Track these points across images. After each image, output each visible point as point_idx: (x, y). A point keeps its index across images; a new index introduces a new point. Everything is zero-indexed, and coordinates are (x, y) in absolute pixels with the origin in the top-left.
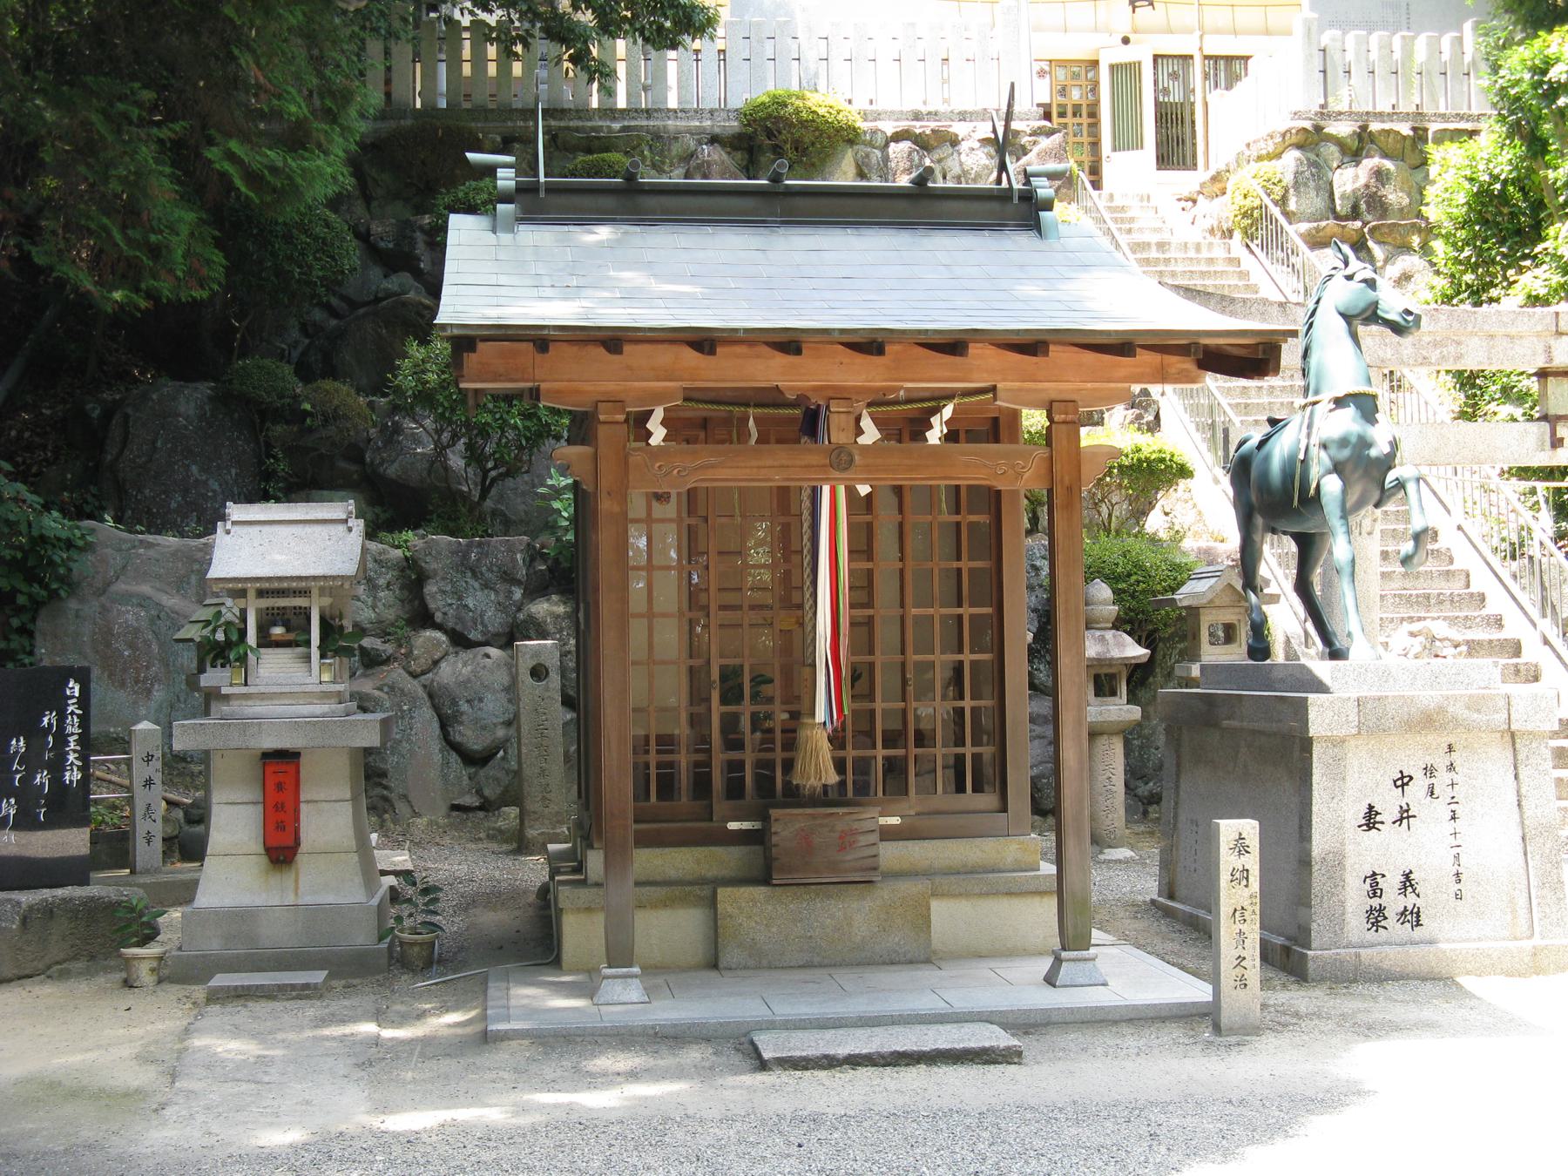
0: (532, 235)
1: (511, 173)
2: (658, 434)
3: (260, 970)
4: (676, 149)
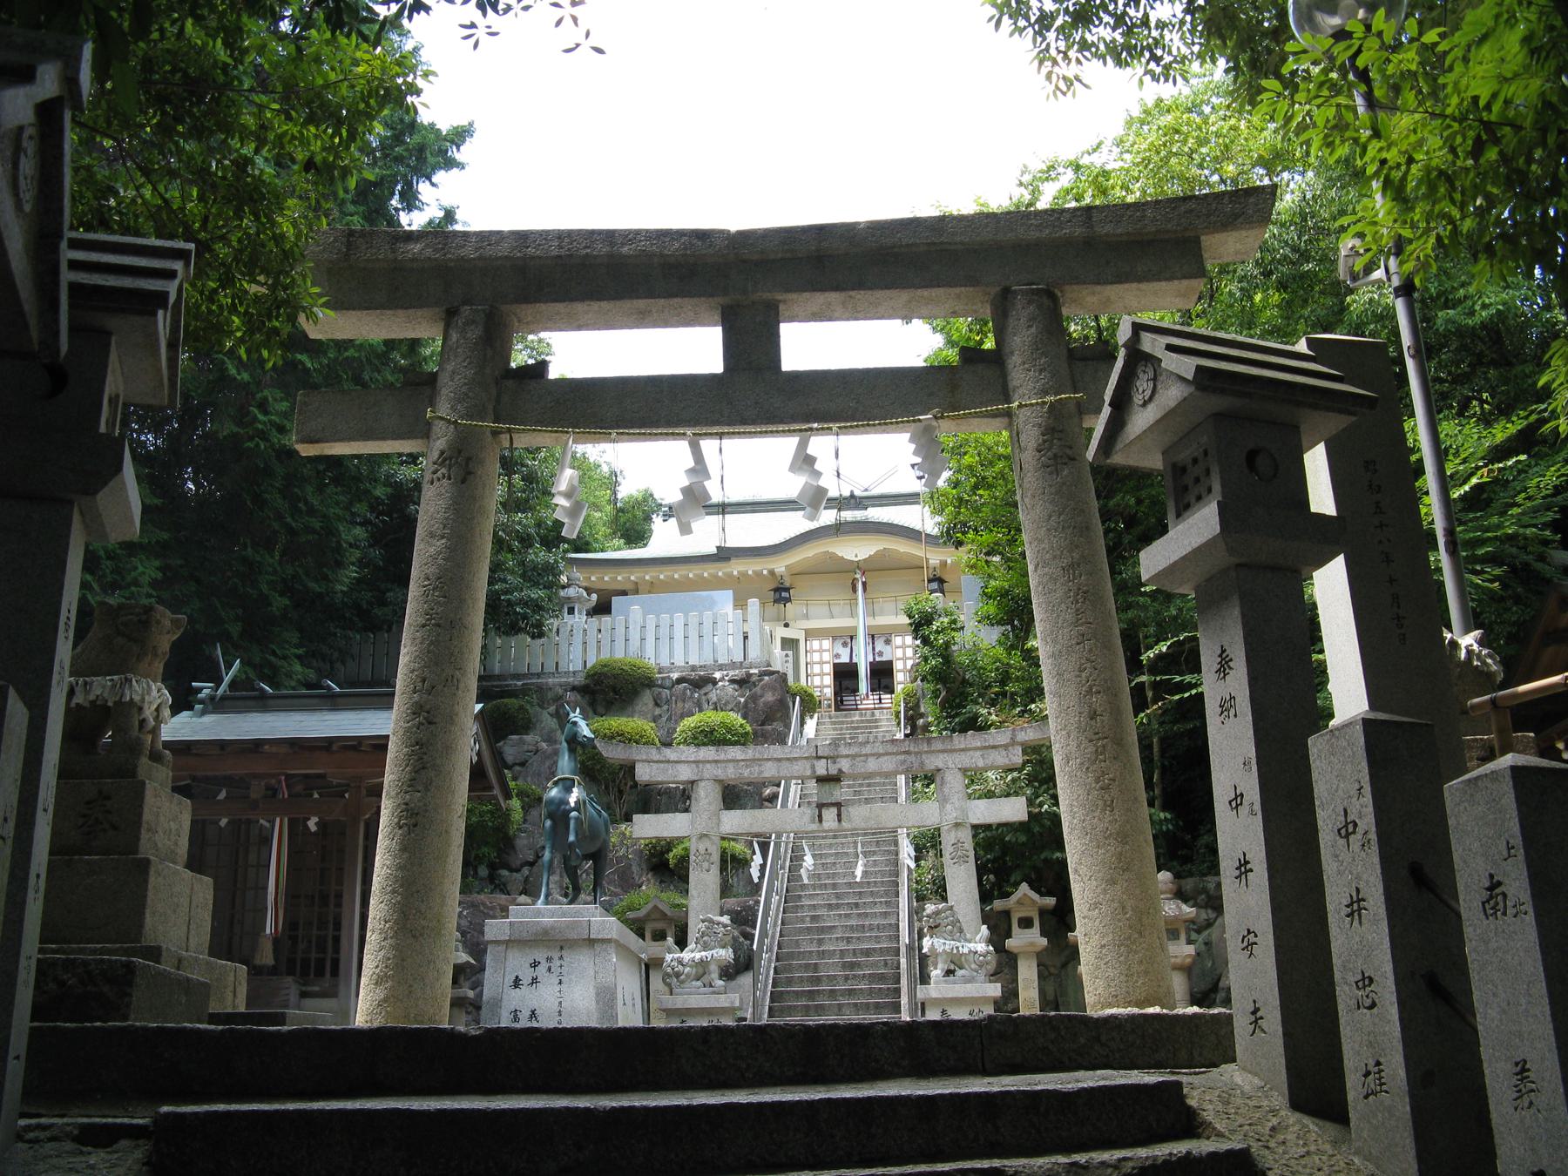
4: (550, 695)
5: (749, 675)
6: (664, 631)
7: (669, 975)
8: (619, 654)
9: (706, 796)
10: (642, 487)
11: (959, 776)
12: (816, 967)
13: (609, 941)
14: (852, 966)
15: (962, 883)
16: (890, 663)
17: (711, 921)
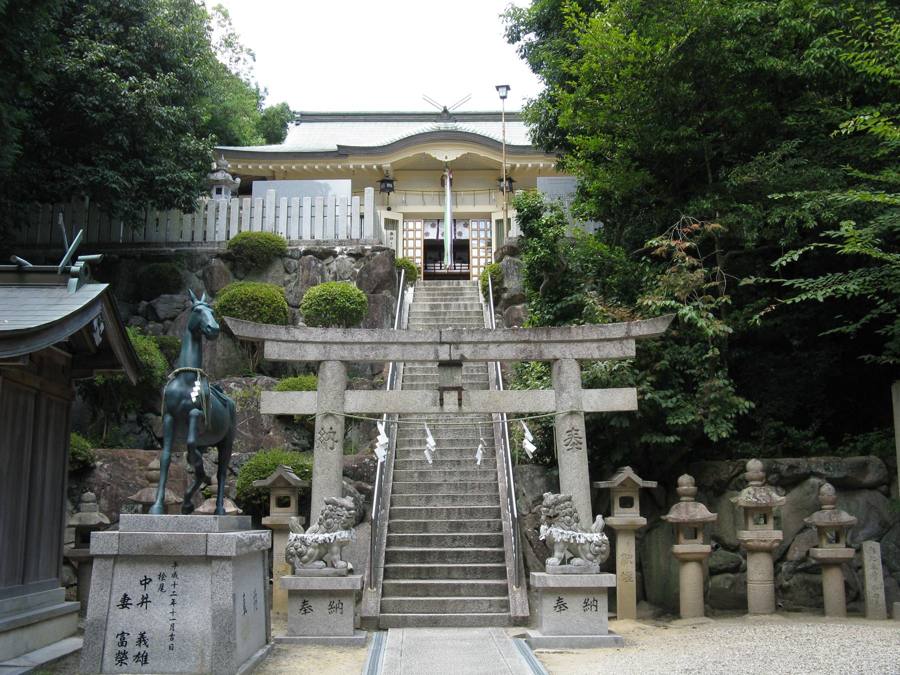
4: (198, 260)
5: (364, 250)
6: (294, 211)
7: (292, 555)
8: (257, 229)
9: (332, 374)
10: (280, 102)
11: (576, 367)
12: (425, 527)
13: (228, 558)
14: (458, 526)
15: (574, 466)
16: (468, 240)
17: (334, 503)
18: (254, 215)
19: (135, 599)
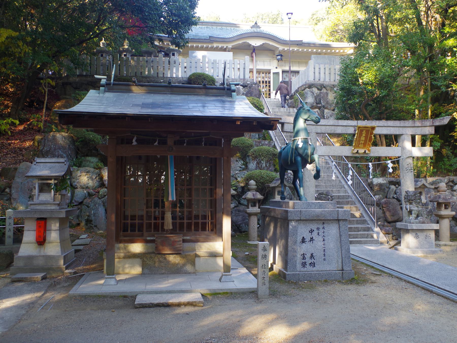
0: (108, 95)
1: (105, 80)
2: (134, 143)
3: (26, 272)
18: (313, 69)
19: (308, 239)
